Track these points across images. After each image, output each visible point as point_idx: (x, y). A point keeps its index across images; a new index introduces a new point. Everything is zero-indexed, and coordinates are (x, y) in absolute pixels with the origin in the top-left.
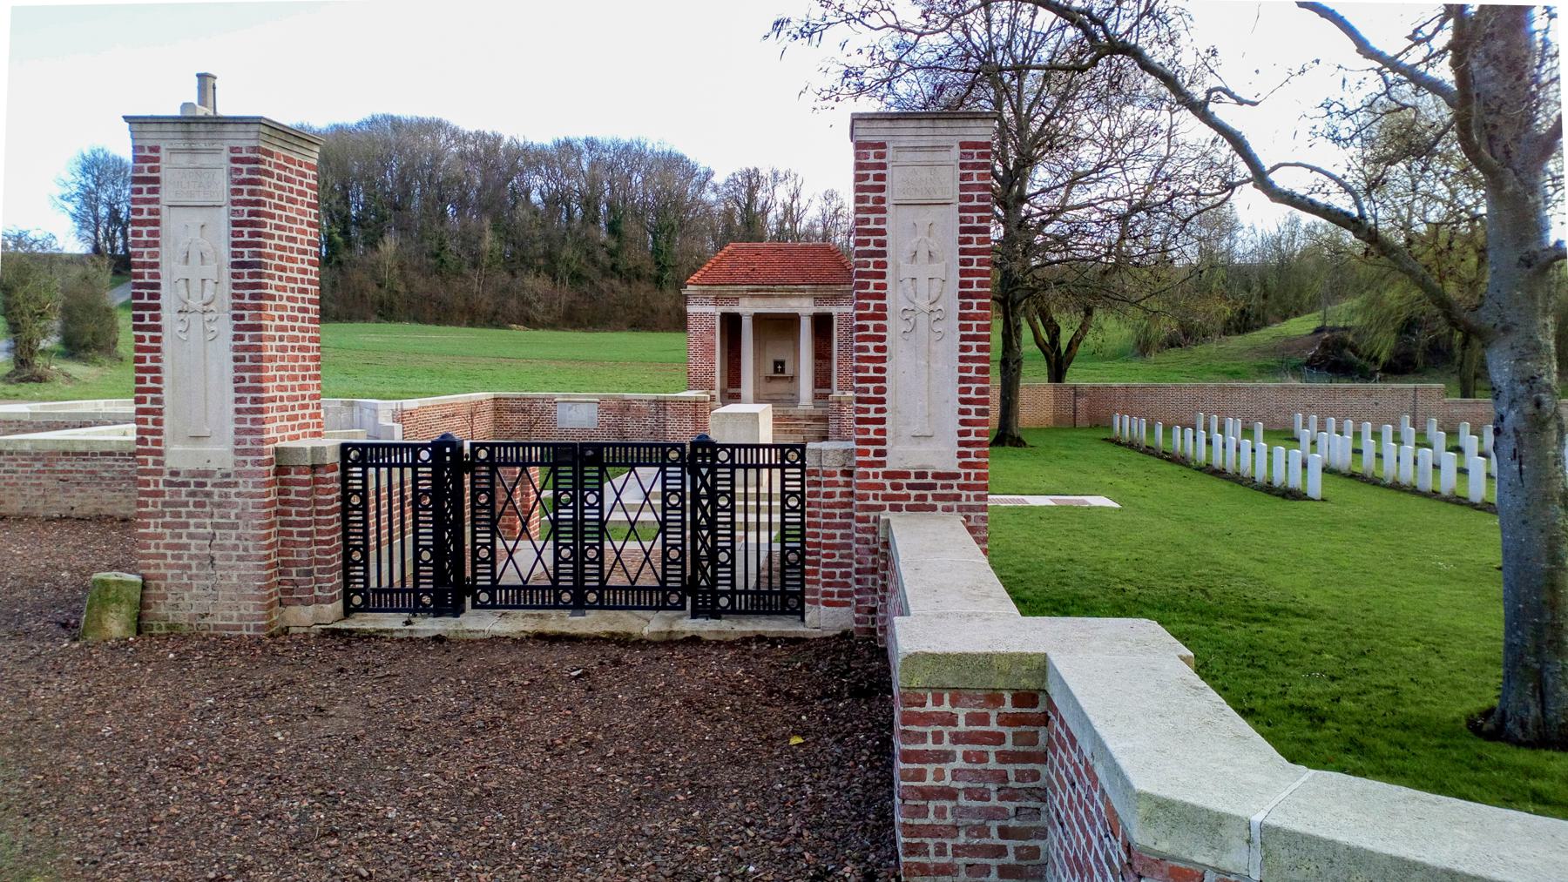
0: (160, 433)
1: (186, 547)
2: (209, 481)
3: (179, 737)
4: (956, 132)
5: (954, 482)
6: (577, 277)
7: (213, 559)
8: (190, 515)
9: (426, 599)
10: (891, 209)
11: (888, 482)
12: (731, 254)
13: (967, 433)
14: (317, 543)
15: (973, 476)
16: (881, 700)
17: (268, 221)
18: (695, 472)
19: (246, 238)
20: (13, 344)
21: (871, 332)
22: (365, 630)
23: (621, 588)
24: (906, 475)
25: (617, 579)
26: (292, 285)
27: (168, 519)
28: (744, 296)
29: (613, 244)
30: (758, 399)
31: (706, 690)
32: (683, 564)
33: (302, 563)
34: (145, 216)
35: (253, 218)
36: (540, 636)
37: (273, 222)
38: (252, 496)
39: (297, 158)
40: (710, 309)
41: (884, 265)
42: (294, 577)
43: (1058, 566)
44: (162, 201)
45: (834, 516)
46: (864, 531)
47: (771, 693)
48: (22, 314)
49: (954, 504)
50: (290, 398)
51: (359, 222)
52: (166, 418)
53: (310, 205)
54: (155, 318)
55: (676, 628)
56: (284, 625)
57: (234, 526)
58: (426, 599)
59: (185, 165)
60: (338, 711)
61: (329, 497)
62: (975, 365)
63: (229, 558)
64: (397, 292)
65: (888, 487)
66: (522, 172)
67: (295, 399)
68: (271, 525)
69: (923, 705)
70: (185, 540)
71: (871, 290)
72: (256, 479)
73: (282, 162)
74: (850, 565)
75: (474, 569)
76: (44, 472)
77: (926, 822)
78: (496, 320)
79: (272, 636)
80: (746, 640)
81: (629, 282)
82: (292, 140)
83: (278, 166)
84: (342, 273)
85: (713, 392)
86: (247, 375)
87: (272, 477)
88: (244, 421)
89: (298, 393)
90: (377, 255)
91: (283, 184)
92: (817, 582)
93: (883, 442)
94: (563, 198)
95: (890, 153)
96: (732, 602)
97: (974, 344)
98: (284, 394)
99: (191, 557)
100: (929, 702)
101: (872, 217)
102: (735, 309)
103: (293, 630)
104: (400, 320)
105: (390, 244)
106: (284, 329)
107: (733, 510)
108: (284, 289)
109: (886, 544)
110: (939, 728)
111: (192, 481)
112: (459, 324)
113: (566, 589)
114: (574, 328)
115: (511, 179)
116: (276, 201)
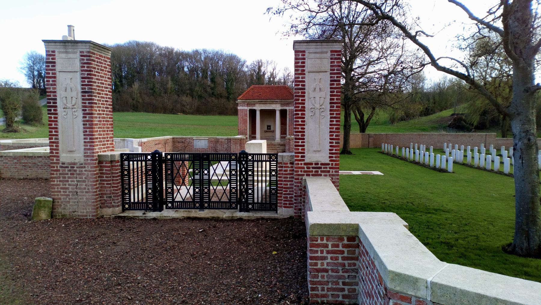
0: (58, 150)
1: (68, 188)
2: (75, 166)
3: (66, 253)
4: (329, 47)
5: (328, 166)
6: (200, 97)
7: (77, 192)
8: (69, 178)
9: (150, 206)
10: (307, 74)
11: (305, 166)
12: (252, 89)
13: (332, 150)
14: (113, 187)
15: (334, 164)
16: (303, 239)
17: (94, 77)
18: (241, 163)
19: (86, 83)
20: (5, 119)
21: (300, 116)
22: (129, 216)
23: (216, 202)
24: (311, 164)
25: (214, 199)
26: (103, 99)
27: (61, 179)
28: (257, 103)
29: (212, 85)
30: (262, 139)
31: (244, 236)
32: (237, 194)
33: (108, 194)
34: (51, 75)
35: (89, 76)
36: (189, 218)
37: (96, 77)
38: (90, 171)
39: (103, 55)
40: (246, 108)
41: (304, 93)
42: (105, 198)
43: (363, 195)
44: (57, 70)
45: (287, 178)
46: (297, 183)
47: (266, 237)
48: (8, 109)
49: (328, 174)
50: (103, 138)
51: (126, 77)
52: (60, 145)
53: (108, 72)
54: (55, 110)
55: (234, 215)
56: (102, 215)
57: (84, 181)
58: (150, 206)
59: (65, 57)
60: (120, 243)
61: (117, 171)
62: (335, 127)
63: (83, 192)
64: (139, 102)
65: (306, 168)
66: (181, 61)
67: (105, 138)
68: (97, 181)
69: (317, 241)
70: (67, 186)
71: (300, 101)
72: (92, 165)
73: (98, 57)
74: (293, 194)
75: (166, 195)
76: (17, 163)
77: (318, 280)
78: (173, 111)
79: (98, 218)
80: (258, 219)
81: (218, 98)
82: (101, 49)
83: (97, 58)
84: (120, 95)
85: (247, 136)
86: (88, 130)
87: (97, 165)
88: (87, 146)
89: (106, 136)
90: (132, 89)
91: (99, 64)
92: (281, 200)
93: (304, 153)
94: (195, 69)
95: (307, 54)
96: (253, 206)
97: (335, 120)
98: (101, 137)
99: (69, 192)
100: (319, 240)
101: (300, 76)
102: (254, 108)
103: (105, 216)
104: (140, 112)
105: (136, 85)
106: (100, 114)
107: (253, 176)
108: (100, 101)
109: (305, 187)
110: (322, 249)
111: (69, 166)
112: (160, 113)
113: (197, 202)
114: (200, 114)
115: (178, 63)
116: (97, 70)
